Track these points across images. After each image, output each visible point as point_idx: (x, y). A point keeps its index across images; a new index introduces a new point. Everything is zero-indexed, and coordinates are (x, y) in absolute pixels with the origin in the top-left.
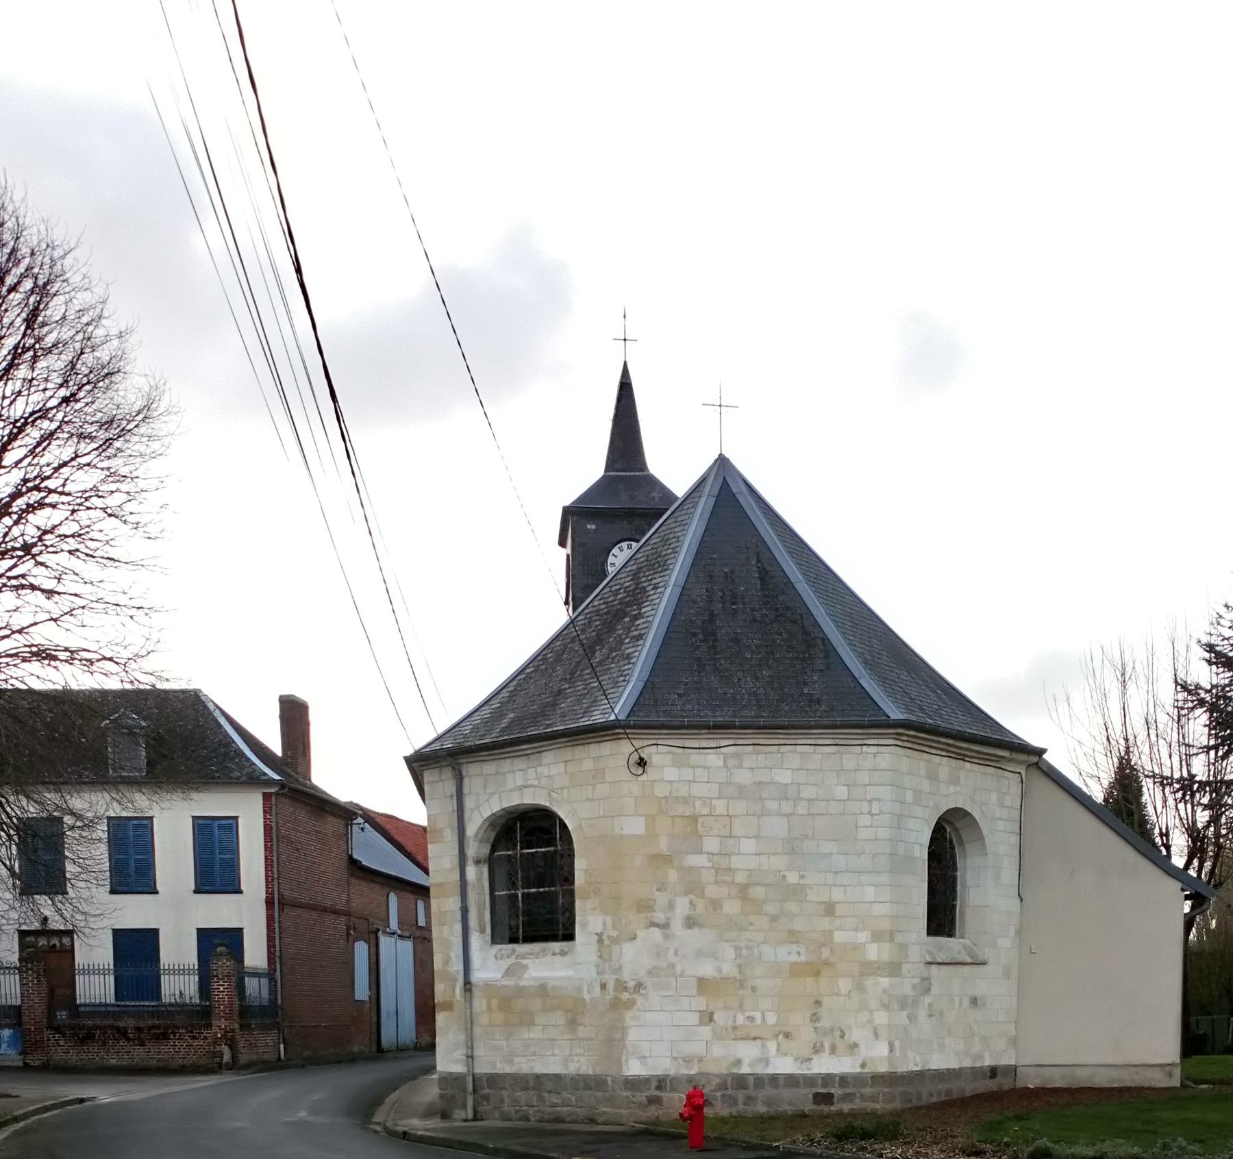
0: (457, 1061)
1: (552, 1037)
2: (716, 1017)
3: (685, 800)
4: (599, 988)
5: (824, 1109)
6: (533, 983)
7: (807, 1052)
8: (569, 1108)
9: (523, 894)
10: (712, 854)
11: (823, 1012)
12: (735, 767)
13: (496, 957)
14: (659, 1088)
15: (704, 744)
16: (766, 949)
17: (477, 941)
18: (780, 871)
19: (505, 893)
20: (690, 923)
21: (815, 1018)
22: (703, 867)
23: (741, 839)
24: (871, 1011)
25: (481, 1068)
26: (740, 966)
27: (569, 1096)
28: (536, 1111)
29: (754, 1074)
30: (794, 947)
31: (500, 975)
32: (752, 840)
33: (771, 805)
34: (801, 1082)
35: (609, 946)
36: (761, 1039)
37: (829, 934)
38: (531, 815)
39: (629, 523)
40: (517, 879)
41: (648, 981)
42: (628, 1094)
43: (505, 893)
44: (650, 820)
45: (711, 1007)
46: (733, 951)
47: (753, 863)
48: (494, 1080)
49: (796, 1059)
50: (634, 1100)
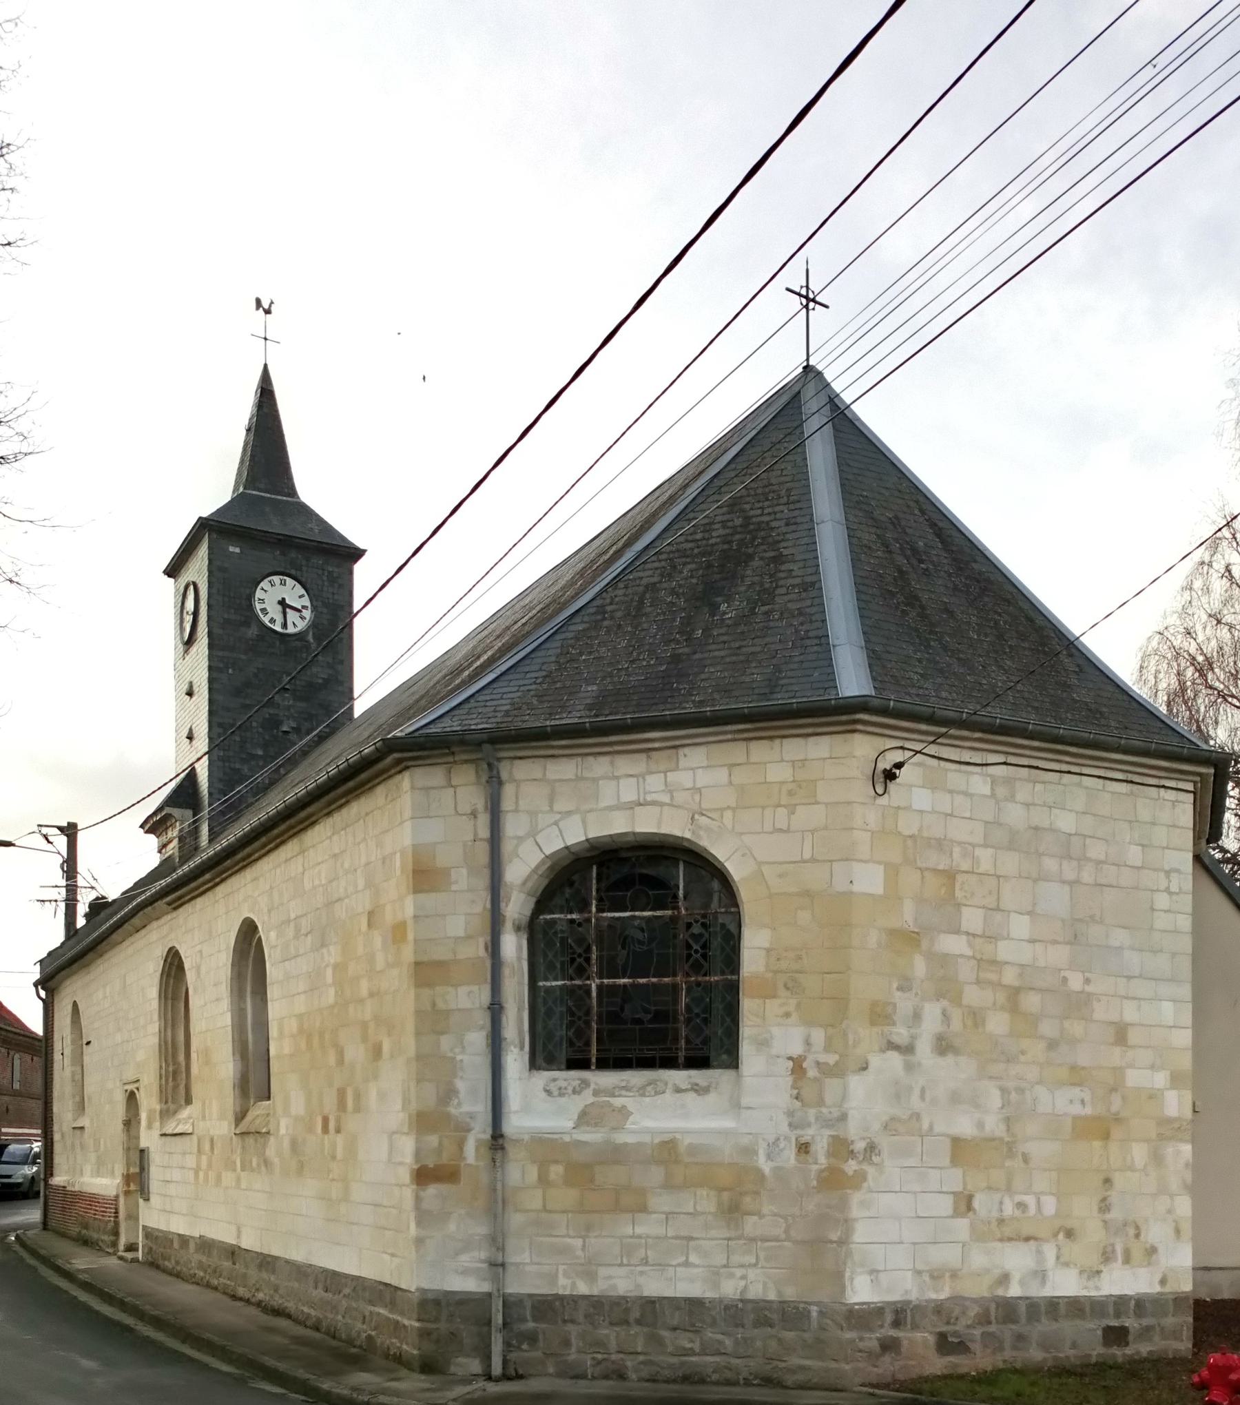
0: (465, 1272)
1: (684, 1233)
2: (976, 1204)
3: (940, 844)
4: (794, 1150)
5: (1119, 1353)
6: (647, 1139)
7: (1093, 1260)
8: (717, 1359)
9: (599, 988)
10: (974, 935)
11: (1114, 1196)
12: (1006, 800)
13: (548, 1092)
14: (897, 1324)
15: (967, 756)
16: (1042, 1093)
17: (515, 1061)
18: (1060, 970)
19: (559, 983)
20: (943, 1046)
21: (1105, 1206)
22: (962, 956)
23: (1012, 915)
24: (1172, 1196)
25: (516, 1286)
26: (1007, 1120)
27: (720, 1337)
28: (642, 1363)
29: (1027, 1298)
30: (1076, 1092)
31: (571, 1124)
32: (1026, 917)
33: (1050, 864)
34: (1088, 1309)
35: (816, 1079)
36: (1036, 1239)
37: (1118, 1072)
38: (624, 855)
40: (588, 960)
41: (884, 1142)
43: (559, 983)
44: (892, 872)
45: (969, 1187)
47: (1025, 954)
49: (1081, 1272)
50: (861, 1345)
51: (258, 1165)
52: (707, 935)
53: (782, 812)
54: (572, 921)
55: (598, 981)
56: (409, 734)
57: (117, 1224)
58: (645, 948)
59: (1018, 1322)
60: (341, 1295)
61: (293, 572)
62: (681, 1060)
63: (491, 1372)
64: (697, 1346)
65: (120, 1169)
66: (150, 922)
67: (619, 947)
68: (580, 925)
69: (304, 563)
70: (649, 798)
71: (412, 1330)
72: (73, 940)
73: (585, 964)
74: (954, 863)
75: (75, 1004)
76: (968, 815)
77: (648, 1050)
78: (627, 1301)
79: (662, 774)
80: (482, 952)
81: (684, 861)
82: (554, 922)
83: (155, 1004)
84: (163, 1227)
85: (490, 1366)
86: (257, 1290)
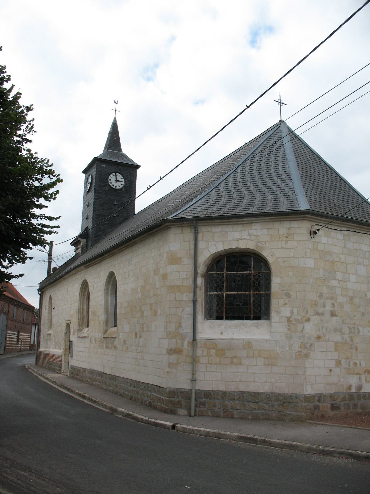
3: (330, 254)
9: (227, 295)
14: (319, 401)
17: (200, 317)
18: (364, 291)
19: (214, 293)
28: (239, 412)
39: (117, 167)
40: (223, 286)
42: (306, 404)
43: (214, 293)
46: (348, 330)
48: (208, 394)
50: (308, 407)
51: (111, 347)
52: (260, 279)
53: (284, 243)
54: (218, 274)
55: (226, 293)
56: (171, 218)
57: (61, 364)
58: (241, 283)
59: (354, 400)
60: (140, 388)
61: (120, 172)
62: (252, 317)
63: (191, 414)
64: (257, 407)
65: (63, 347)
66: (78, 272)
67: (233, 282)
68: (221, 275)
69: (123, 169)
70: (243, 238)
71: (165, 400)
72: (50, 277)
73: (222, 287)
74: (334, 259)
75: (50, 297)
76: (337, 245)
77: (241, 314)
78: (235, 393)
79: (247, 231)
80: (191, 283)
81: (253, 257)
82: (212, 274)
83: (78, 297)
84: (77, 366)
85: (191, 412)
86: (110, 386)
